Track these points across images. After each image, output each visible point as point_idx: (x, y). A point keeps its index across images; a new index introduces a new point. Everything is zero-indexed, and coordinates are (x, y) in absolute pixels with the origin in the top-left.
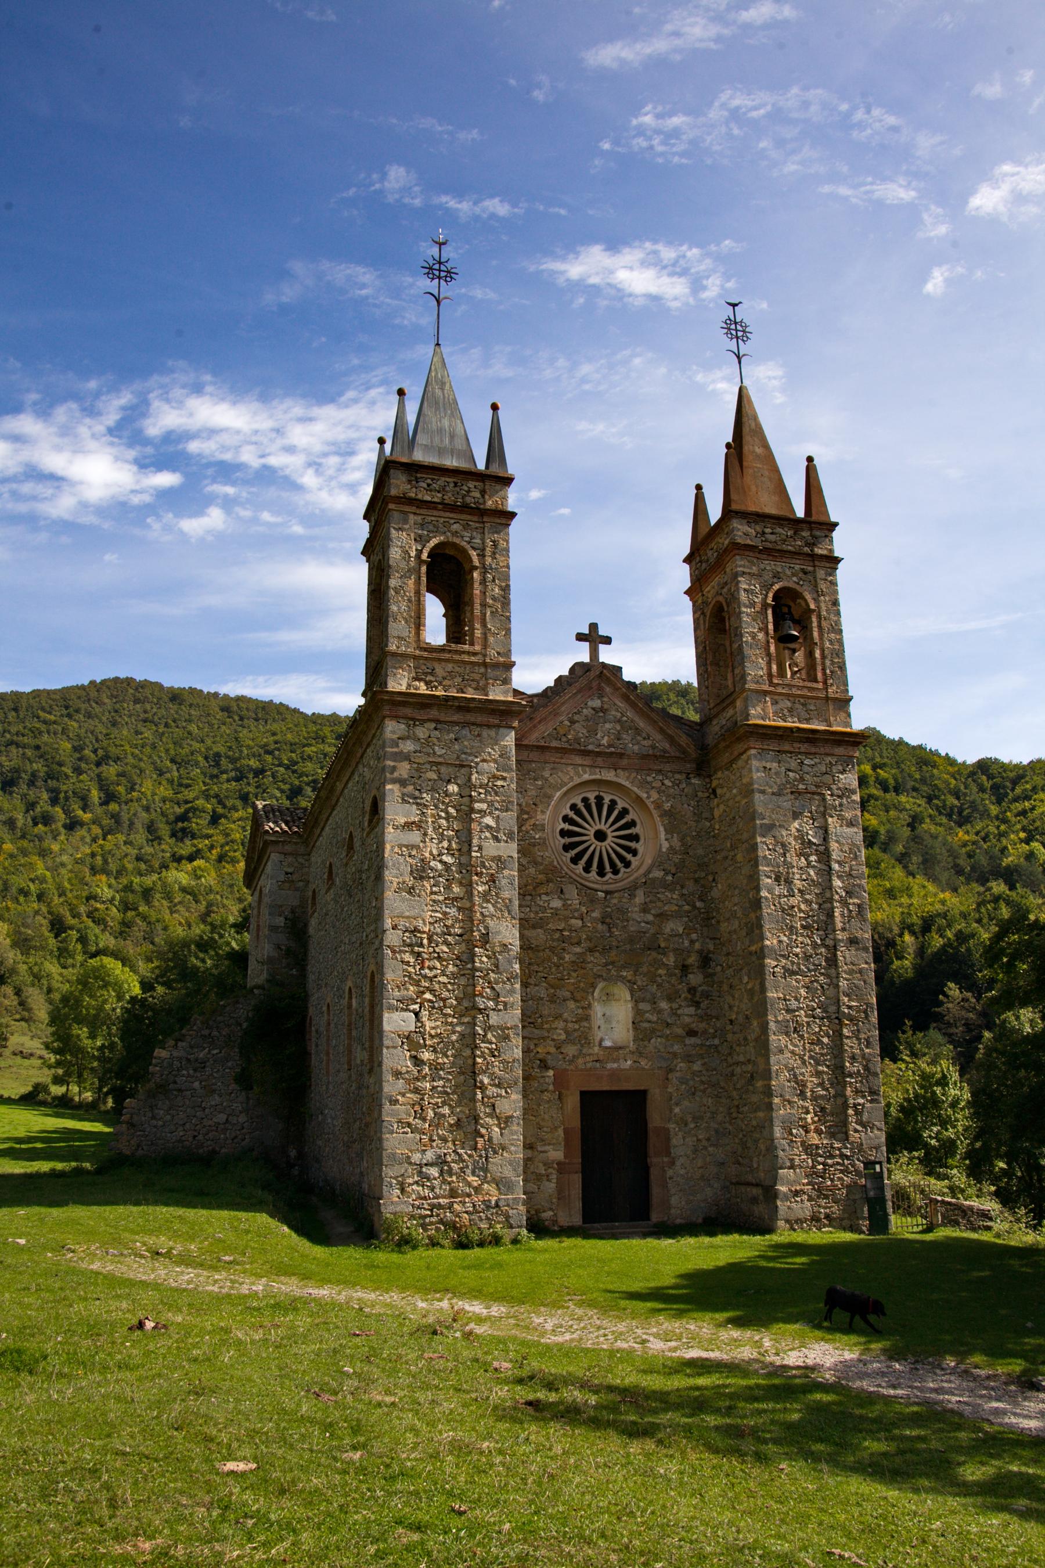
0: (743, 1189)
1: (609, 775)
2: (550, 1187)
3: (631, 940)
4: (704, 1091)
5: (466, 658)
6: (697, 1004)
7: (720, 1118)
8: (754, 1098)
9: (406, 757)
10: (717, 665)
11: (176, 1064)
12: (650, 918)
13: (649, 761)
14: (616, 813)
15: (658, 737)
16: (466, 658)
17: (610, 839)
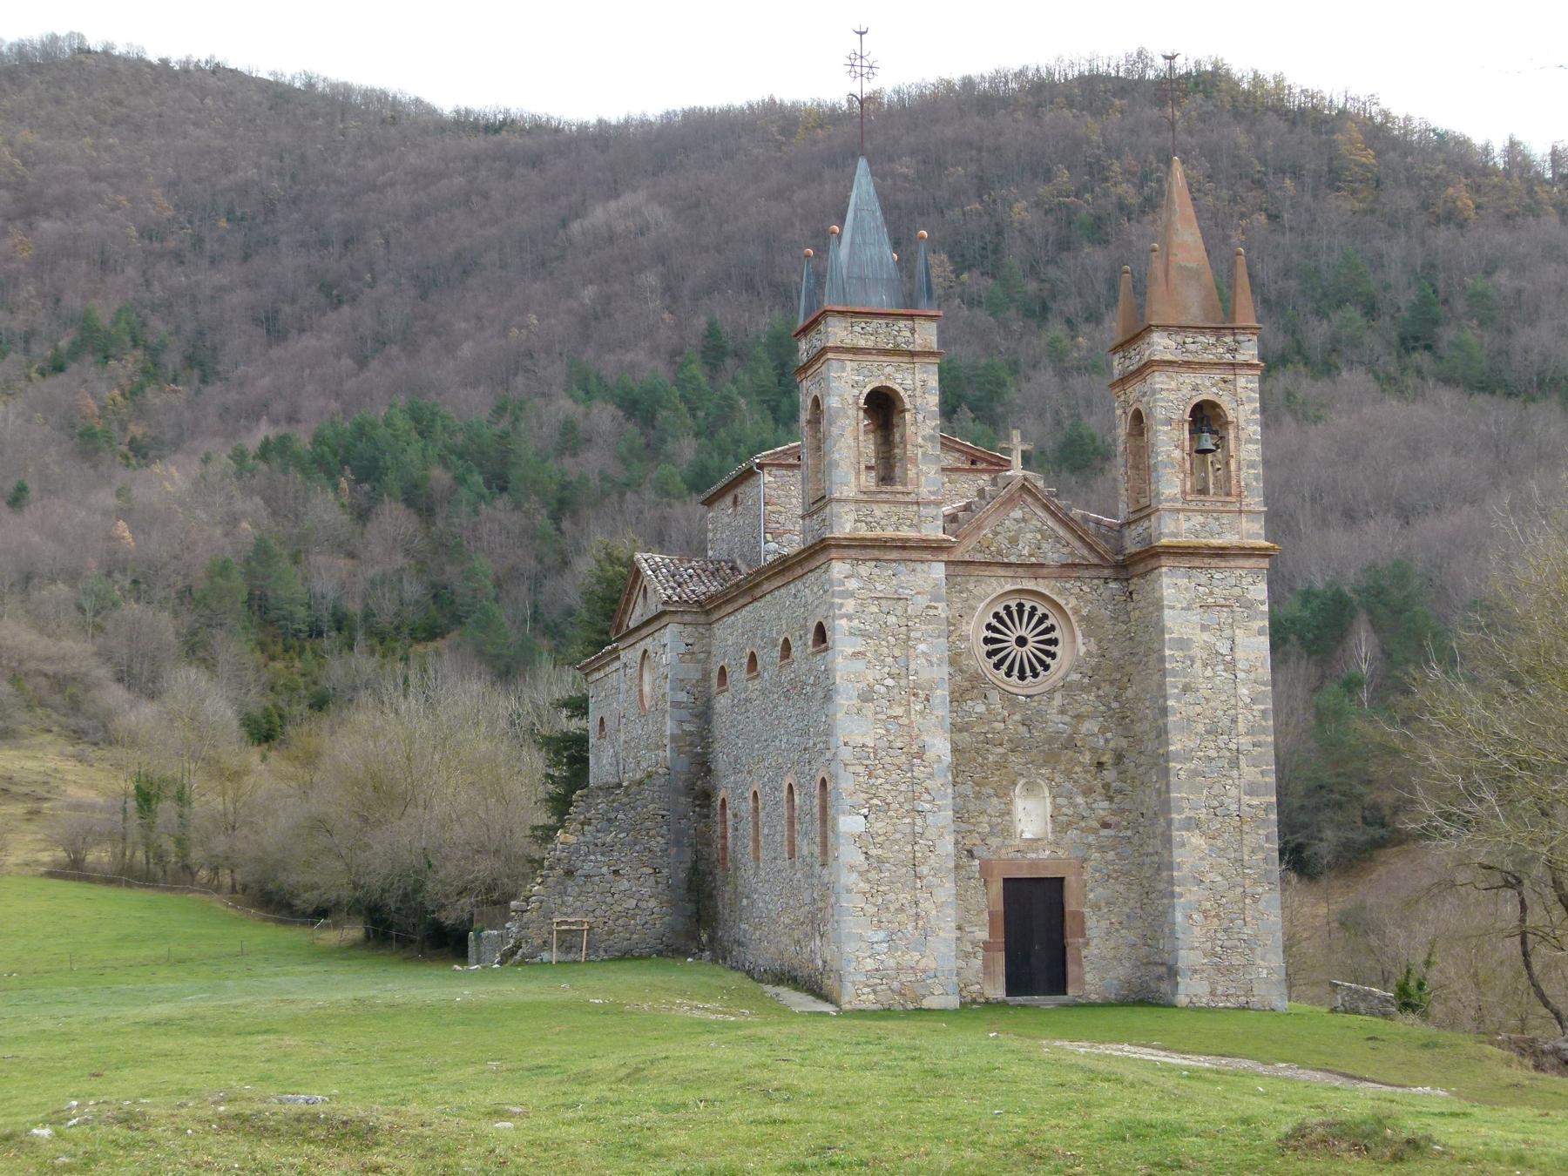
0: (1151, 968)
1: (1030, 585)
2: (977, 963)
3: (1050, 741)
4: (1116, 879)
5: (900, 498)
6: (1111, 799)
7: (1132, 903)
8: (1161, 886)
9: (852, 595)
10: (1137, 468)
11: (584, 849)
12: (1067, 719)
13: (1069, 568)
14: (1035, 619)
15: (1077, 544)
16: (900, 498)
17: (1030, 640)
